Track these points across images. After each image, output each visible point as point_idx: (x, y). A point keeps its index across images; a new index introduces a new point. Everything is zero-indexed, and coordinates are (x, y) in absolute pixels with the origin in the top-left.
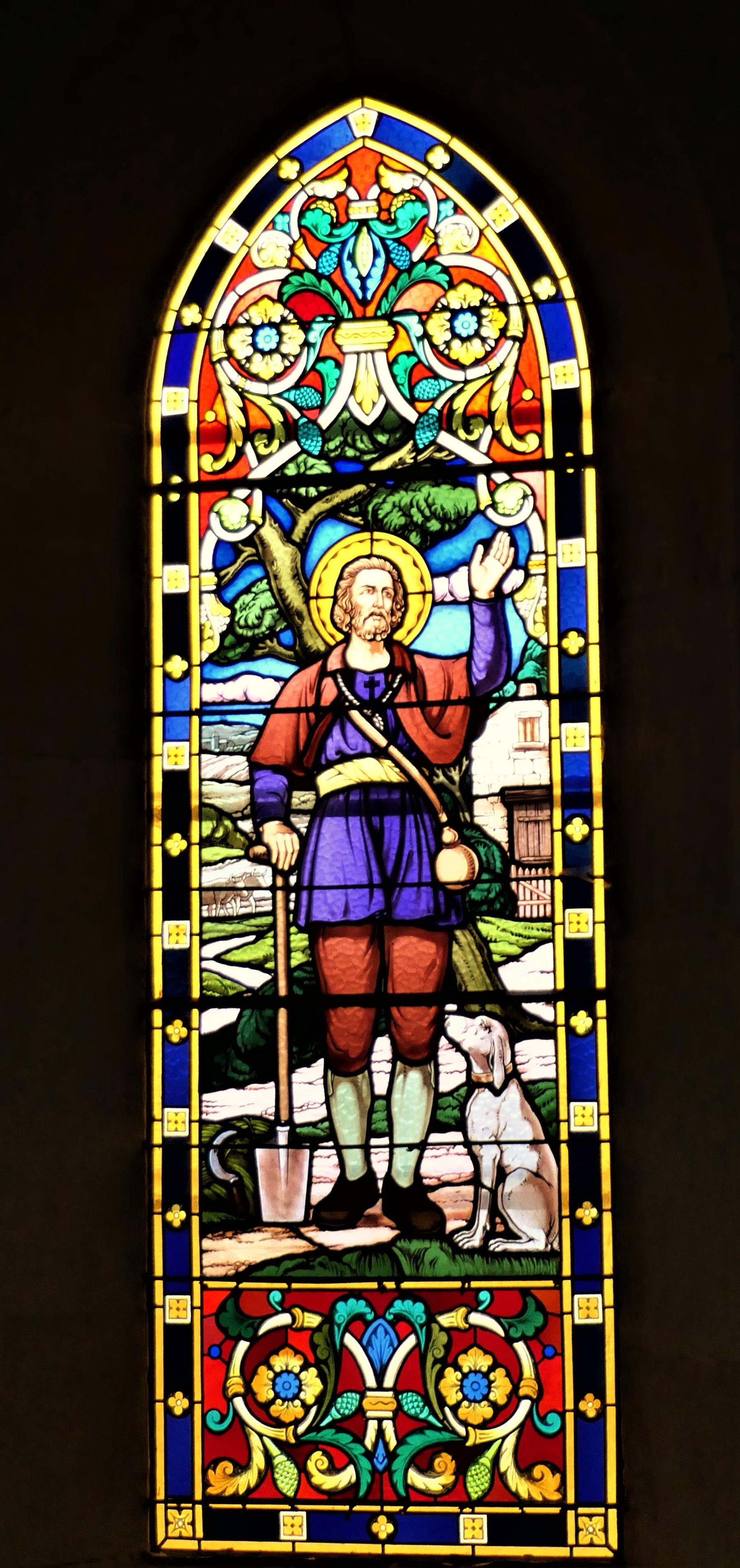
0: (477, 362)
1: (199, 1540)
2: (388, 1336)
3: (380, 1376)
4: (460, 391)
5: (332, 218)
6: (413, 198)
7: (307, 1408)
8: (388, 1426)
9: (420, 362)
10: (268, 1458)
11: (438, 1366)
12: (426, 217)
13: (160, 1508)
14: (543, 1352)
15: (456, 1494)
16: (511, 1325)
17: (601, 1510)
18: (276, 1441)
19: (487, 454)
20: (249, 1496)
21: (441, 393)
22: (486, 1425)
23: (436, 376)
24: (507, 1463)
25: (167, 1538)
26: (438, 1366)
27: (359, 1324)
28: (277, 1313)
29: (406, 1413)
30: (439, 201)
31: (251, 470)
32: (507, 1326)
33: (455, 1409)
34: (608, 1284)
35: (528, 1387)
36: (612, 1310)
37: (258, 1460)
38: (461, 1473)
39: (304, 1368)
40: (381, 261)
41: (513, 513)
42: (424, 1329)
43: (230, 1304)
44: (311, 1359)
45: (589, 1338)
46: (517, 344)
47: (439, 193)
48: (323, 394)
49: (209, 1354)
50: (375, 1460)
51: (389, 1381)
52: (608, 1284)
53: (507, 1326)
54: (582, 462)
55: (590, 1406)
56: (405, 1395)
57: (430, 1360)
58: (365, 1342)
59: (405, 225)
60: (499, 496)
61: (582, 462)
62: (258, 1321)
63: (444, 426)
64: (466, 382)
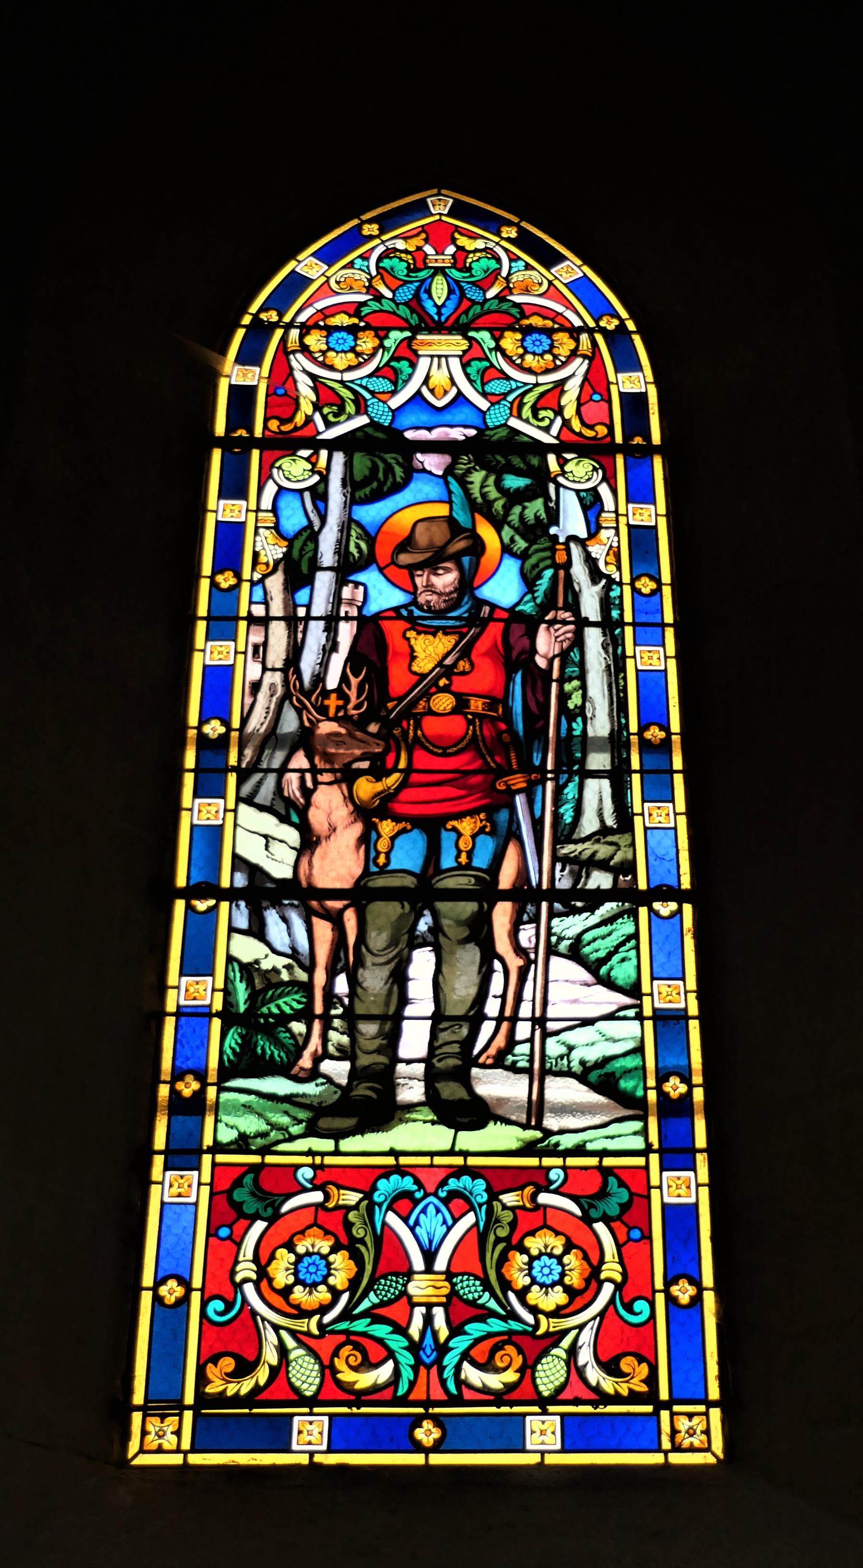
0: (547, 371)
1: (186, 1453)
2: (440, 1215)
3: (429, 1256)
4: (530, 390)
5: (409, 264)
6: (489, 256)
7: (336, 1294)
8: (439, 1314)
9: (492, 365)
10: (283, 1351)
11: (500, 1247)
12: (500, 269)
13: (137, 1417)
14: (628, 1234)
15: (525, 1392)
16: (591, 1206)
17: (702, 1408)
18: (293, 1333)
19: (557, 438)
20: (253, 1398)
21: (512, 391)
22: (558, 1313)
23: (508, 378)
24: (585, 1356)
25: (142, 1451)
26: (500, 1247)
27: (405, 1203)
28: (305, 1190)
29: (460, 1298)
30: (511, 260)
31: (319, 433)
32: (586, 1207)
33: (522, 1294)
34: (701, 1160)
35: (612, 1270)
36: (706, 1189)
37: (271, 1356)
38: (528, 1369)
39: (334, 1250)
40: (455, 298)
41: (582, 480)
42: (484, 1208)
43: (248, 1179)
44: (344, 1240)
45: (680, 1219)
46: (587, 362)
47: (511, 255)
48: (396, 387)
49: (216, 1235)
50: (421, 1353)
51: (441, 1264)
52: (701, 1160)
53: (586, 1207)
54: (649, 450)
55: (684, 1292)
56: (460, 1278)
57: (492, 1238)
58: (412, 1222)
59: (479, 273)
60: (567, 468)
61: (649, 450)
62: (282, 1198)
63: (515, 412)
64: (537, 385)
